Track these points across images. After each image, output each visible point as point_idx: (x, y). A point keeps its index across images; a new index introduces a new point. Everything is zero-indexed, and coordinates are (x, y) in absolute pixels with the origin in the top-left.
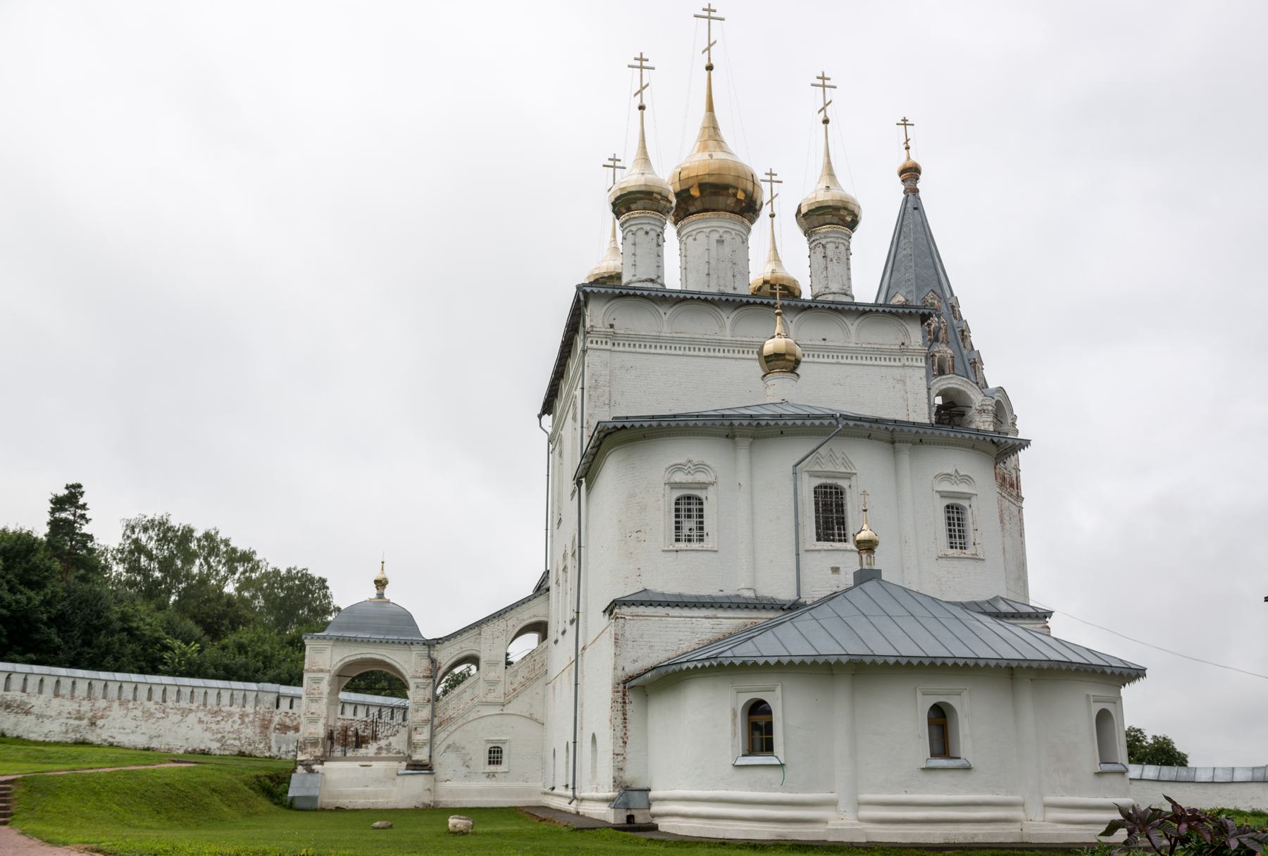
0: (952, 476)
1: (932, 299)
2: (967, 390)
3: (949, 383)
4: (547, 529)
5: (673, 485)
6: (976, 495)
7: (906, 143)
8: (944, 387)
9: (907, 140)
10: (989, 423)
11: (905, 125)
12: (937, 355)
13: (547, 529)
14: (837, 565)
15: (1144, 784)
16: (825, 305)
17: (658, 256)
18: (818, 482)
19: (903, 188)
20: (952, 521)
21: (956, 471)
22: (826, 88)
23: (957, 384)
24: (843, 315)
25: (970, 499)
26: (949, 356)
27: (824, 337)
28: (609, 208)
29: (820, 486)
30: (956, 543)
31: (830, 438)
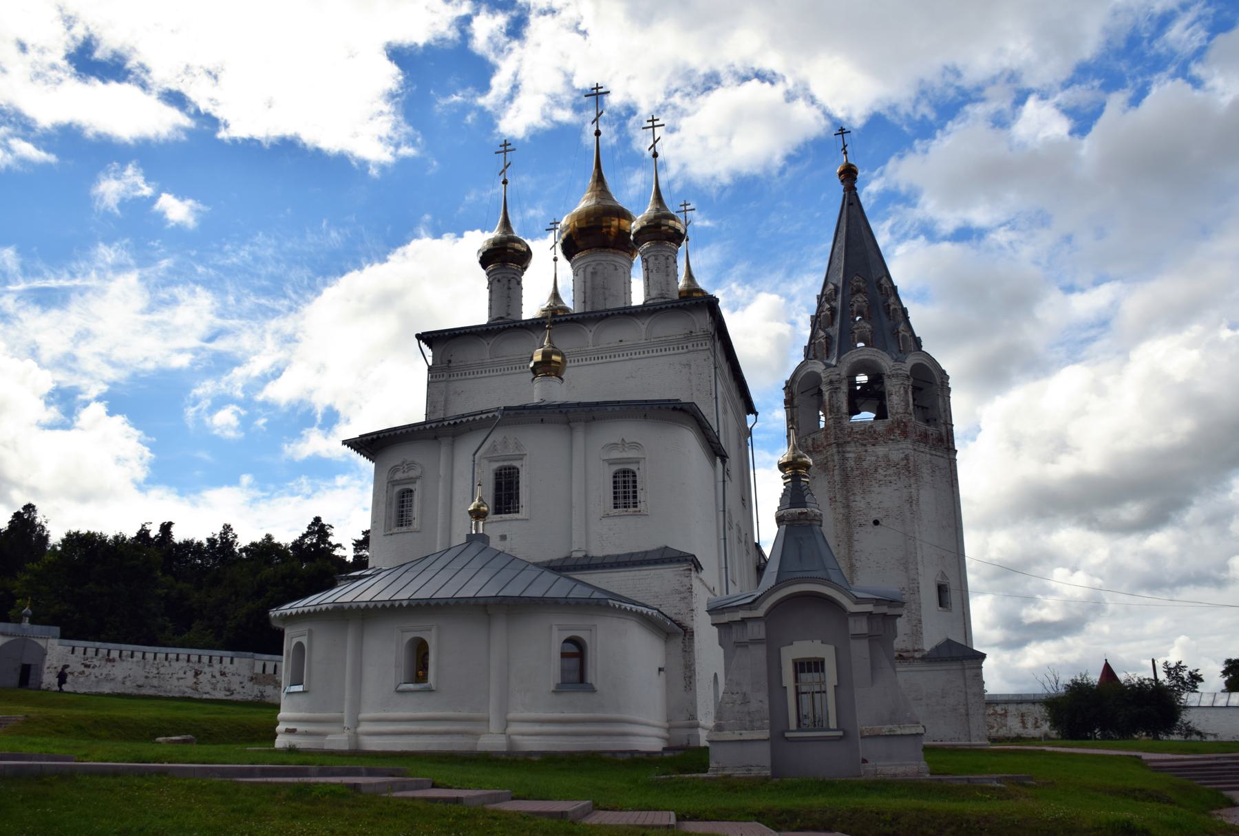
0: (617, 444)
1: (857, 281)
2: (877, 358)
3: (860, 355)
4: (758, 523)
5: (394, 483)
6: (644, 458)
7: (844, 149)
8: (855, 360)
9: (845, 146)
10: (898, 386)
11: (843, 133)
12: (856, 331)
13: (758, 523)
14: (505, 534)
15: (1231, 711)
16: (620, 311)
17: (509, 297)
18: (496, 465)
19: (843, 187)
20: (627, 484)
21: (623, 440)
22: (652, 129)
23: (867, 355)
24: (637, 318)
25: (638, 462)
26: (868, 330)
27: (621, 339)
28: (479, 266)
29: (500, 469)
30: (629, 503)
31: (493, 429)
